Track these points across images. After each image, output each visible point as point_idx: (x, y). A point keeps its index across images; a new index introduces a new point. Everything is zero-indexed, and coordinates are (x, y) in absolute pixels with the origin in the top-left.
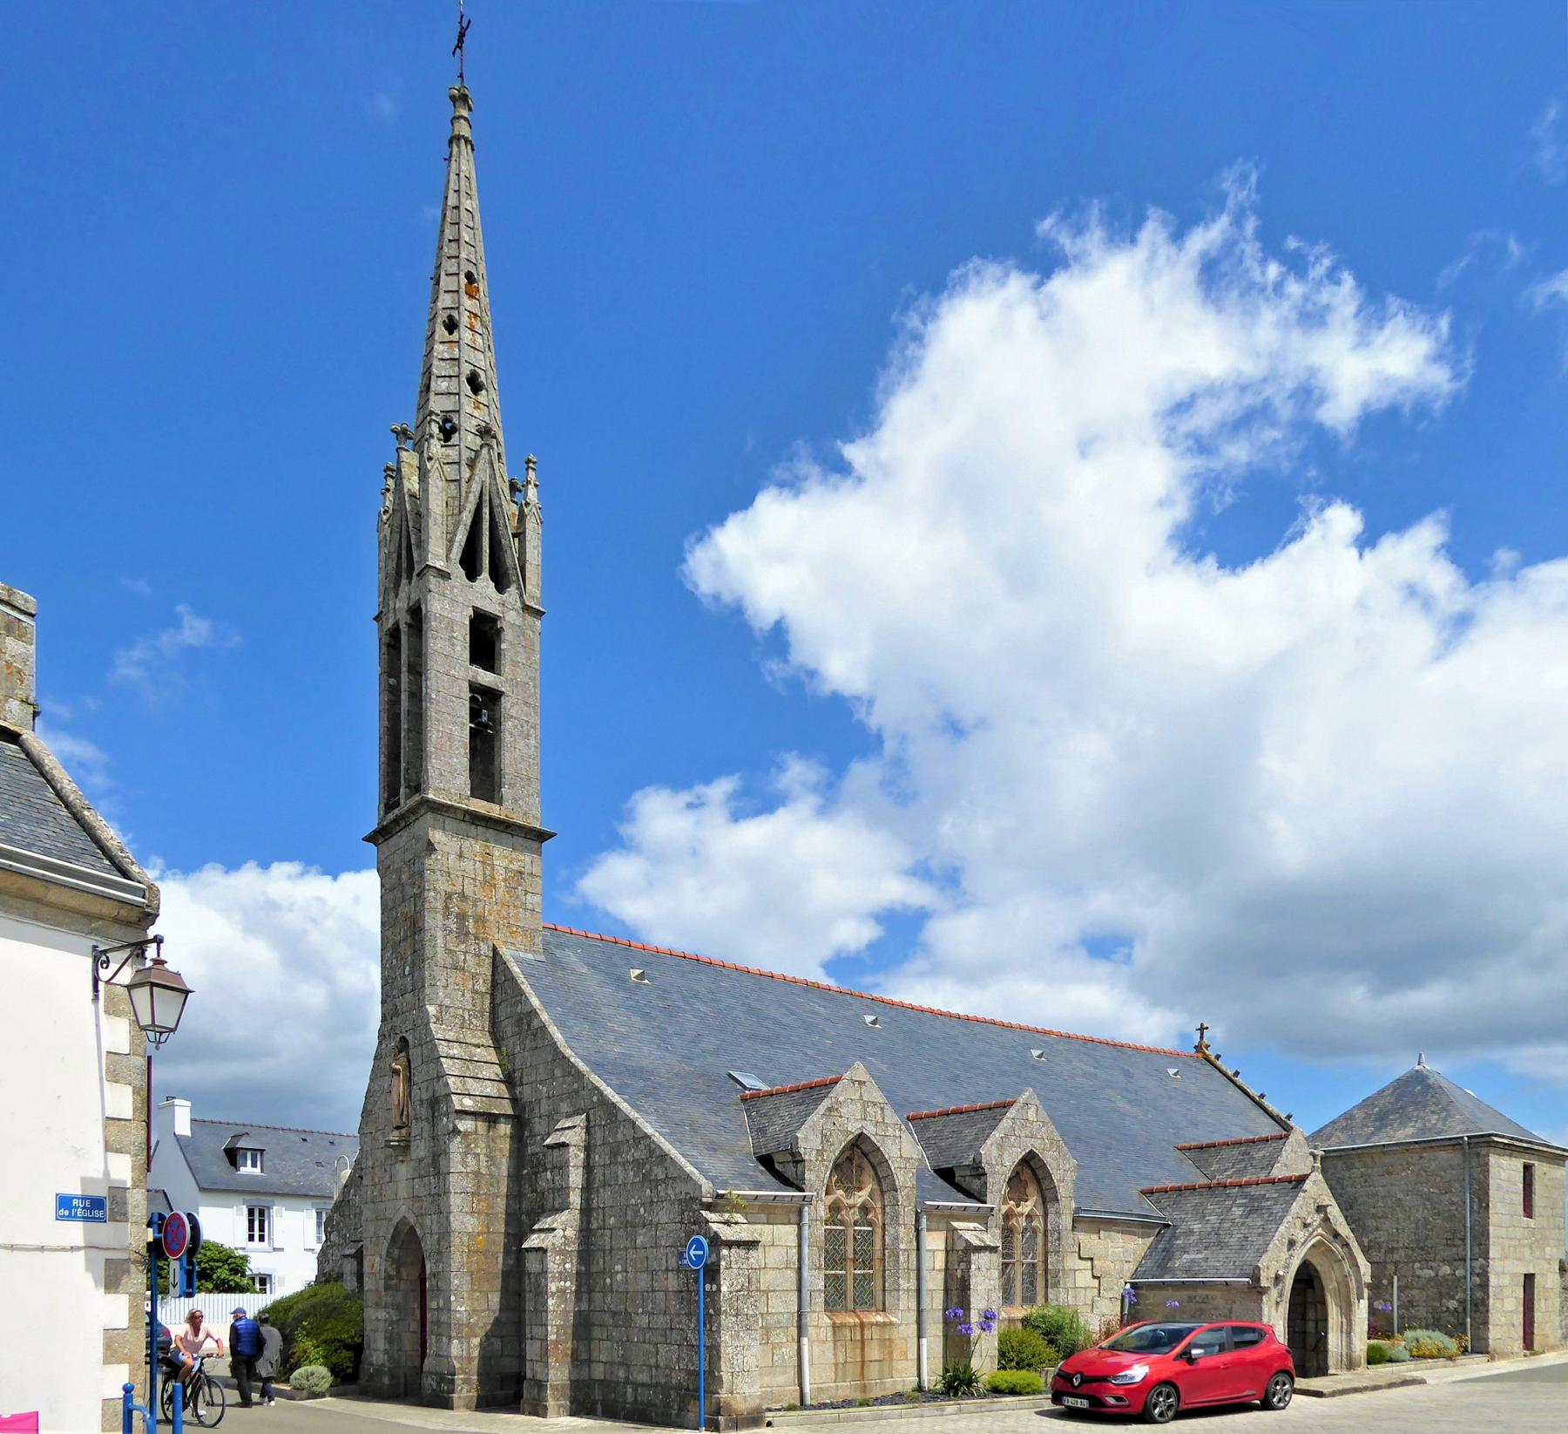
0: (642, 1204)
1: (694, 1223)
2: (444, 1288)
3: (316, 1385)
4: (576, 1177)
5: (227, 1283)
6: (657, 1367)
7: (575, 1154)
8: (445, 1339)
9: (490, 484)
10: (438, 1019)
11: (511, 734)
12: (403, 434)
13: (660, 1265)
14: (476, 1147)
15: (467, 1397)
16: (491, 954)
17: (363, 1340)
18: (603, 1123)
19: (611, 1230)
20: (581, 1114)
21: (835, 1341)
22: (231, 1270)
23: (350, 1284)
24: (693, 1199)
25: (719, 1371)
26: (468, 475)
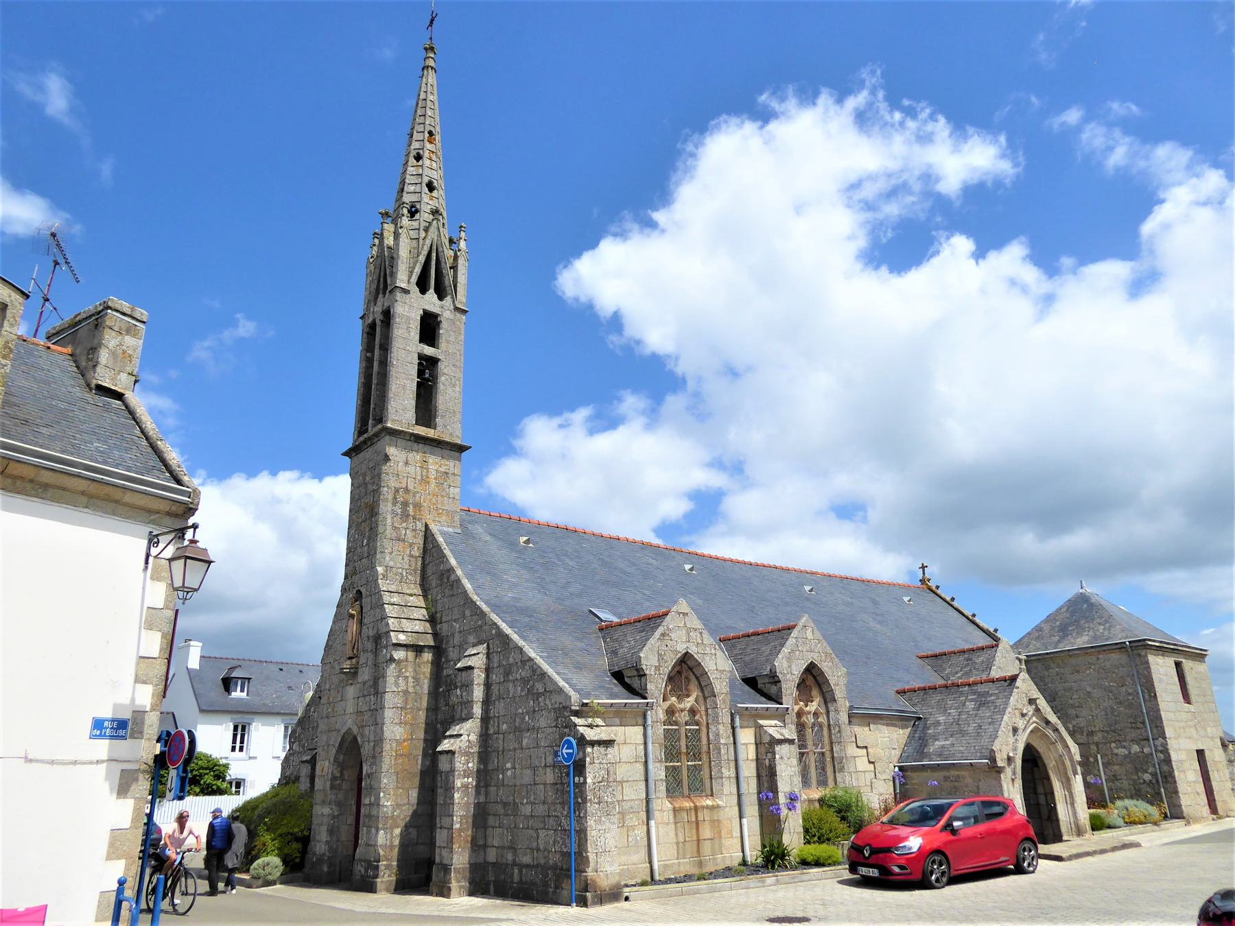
0: (527, 713)
1: (566, 727)
2: (376, 786)
3: (270, 874)
4: (478, 693)
5: (211, 787)
6: (538, 849)
7: (478, 675)
8: (373, 830)
9: (437, 240)
10: (384, 576)
11: (443, 384)
12: (386, 215)
13: (540, 762)
14: (406, 671)
15: (388, 881)
16: (424, 530)
17: (310, 833)
18: (499, 650)
19: (504, 734)
20: (483, 644)
21: (676, 823)
22: (215, 776)
23: (304, 785)
24: (565, 708)
25: (587, 852)
26: (424, 235)
